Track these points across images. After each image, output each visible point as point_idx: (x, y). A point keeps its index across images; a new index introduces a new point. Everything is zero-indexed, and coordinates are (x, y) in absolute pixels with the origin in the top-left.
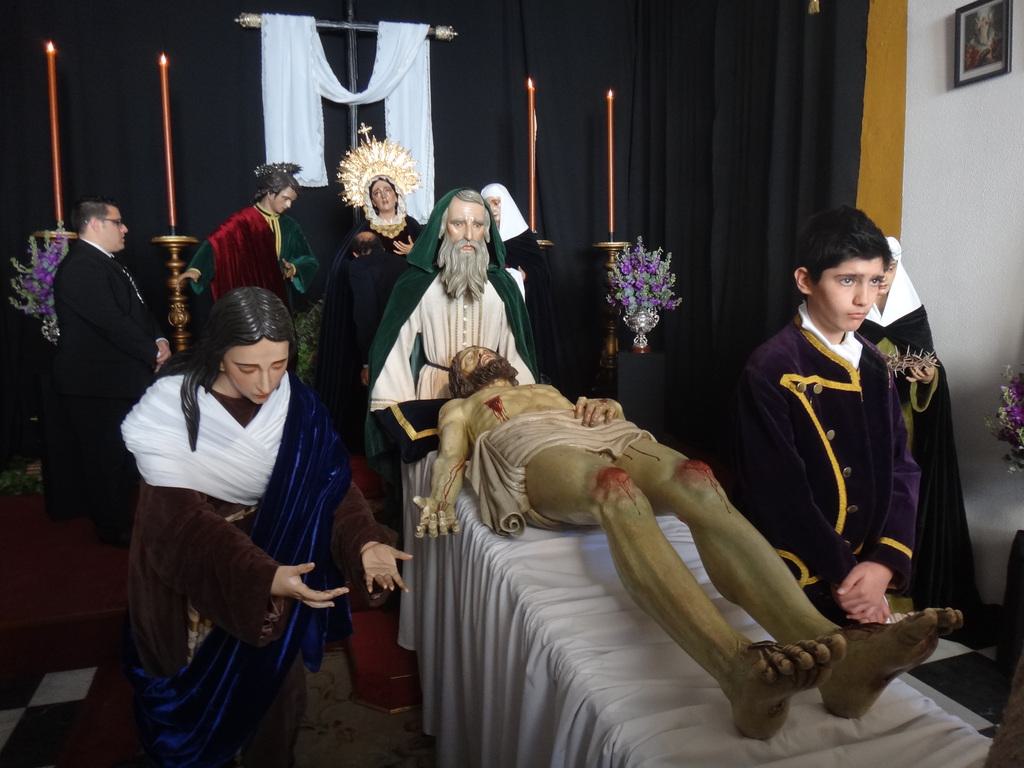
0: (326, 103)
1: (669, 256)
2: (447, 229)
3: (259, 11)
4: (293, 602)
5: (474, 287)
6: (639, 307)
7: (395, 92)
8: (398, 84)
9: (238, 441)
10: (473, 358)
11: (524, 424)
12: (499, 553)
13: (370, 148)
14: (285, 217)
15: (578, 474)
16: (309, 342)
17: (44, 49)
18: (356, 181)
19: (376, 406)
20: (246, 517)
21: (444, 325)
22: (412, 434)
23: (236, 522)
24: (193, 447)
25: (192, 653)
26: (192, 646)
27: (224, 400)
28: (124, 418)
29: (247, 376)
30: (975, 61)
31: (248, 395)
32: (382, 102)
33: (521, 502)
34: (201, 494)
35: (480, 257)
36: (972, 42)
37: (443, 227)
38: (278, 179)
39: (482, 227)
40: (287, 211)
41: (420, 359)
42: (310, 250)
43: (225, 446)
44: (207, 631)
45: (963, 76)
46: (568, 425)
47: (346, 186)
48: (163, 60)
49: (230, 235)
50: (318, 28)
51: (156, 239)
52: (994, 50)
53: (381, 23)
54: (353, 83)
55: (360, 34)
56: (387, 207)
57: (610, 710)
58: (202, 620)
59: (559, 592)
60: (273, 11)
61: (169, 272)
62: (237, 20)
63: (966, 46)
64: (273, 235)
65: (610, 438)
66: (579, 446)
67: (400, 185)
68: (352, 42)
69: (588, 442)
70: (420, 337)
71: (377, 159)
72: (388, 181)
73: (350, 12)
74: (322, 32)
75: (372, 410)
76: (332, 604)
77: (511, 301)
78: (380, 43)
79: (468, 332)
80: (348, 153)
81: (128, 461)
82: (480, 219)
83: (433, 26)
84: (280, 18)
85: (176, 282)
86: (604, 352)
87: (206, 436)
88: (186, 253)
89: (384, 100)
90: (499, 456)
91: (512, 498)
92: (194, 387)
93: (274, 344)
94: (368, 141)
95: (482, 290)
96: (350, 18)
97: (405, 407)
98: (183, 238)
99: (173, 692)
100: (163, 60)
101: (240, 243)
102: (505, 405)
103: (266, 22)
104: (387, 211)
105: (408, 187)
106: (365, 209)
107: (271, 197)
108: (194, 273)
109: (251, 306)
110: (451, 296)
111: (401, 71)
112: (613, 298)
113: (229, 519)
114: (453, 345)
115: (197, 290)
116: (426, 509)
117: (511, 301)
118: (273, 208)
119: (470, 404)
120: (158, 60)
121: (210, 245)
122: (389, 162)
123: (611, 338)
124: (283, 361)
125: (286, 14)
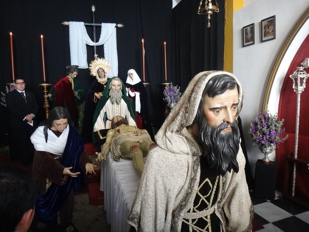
0: (87, 46)
1: (180, 87)
2: (111, 87)
3: (68, 21)
4: (69, 176)
5: (118, 101)
6: (171, 102)
7: (107, 42)
8: (108, 40)
9: (57, 140)
10: (117, 119)
11: (122, 136)
12: (114, 165)
13: (97, 60)
14: (74, 79)
15: (128, 147)
16: (83, 112)
17: (9, 34)
18: (94, 69)
19: (95, 131)
20: (59, 158)
21: (111, 111)
22: (101, 138)
23: (57, 159)
24: (47, 142)
25: (47, 189)
26: (47, 188)
27: (53, 131)
28: (31, 136)
29: (58, 126)
30: (247, 41)
31: (58, 130)
32: (103, 45)
33: (119, 153)
34: (48, 152)
35: (119, 93)
36: (246, 36)
37: (110, 86)
38: (73, 69)
39: (120, 86)
40: (75, 78)
41: (106, 119)
42: (82, 88)
43: (54, 142)
44: (51, 184)
45: (245, 44)
46: (132, 136)
47: (91, 71)
48: (42, 36)
49: (60, 84)
50: (85, 25)
51: (40, 85)
52: (251, 38)
53: (102, 23)
54: (95, 40)
55: (96, 26)
56: (102, 76)
57: (125, 192)
58: (49, 182)
59: (124, 172)
60: (72, 21)
61: (44, 93)
62: (62, 23)
63: (245, 37)
64: (72, 84)
65: (140, 139)
66: (132, 141)
67: (106, 70)
68: (94, 29)
69: (134, 140)
70: (106, 113)
71: (99, 63)
72: (102, 69)
73: (94, 20)
74: (86, 26)
75: (94, 131)
76: (77, 176)
77: (128, 104)
78: (102, 29)
79: (118, 112)
80: (92, 62)
81: (32, 145)
82: (119, 84)
83: (117, 24)
84: (74, 23)
85: (46, 96)
86: (165, 113)
87: (50, 140)
88: (48, 88)
89: (103, 44)
90: (116, 142)
91: (118, 152)
92: (46, 129)
93: (64, 119)
94: (97, 59)
95: (120, 101)
96: (94, 22)
97: (101, 131)
98: (47, 84)
99: (43, 199)
100: (42, 36)
101: (62, 86)
102: (121, 131)
103: (71, 24)
104: (102, 77)
105: (108, 71)
106: (96, 77)
107: (71, 74)
108: (50, 95)
109: (59, 111)
110: (113, 103)
111: (108, 37)
112: (165, 99)
113: (55, 158)
114: (114, 115)
115: (51, 100)
116: (99, 155)
117: (128, 104)
118: (72, 77)
119: (114, 131)
120: (40, 36)
121: (54, 87)
122: (103, 64)
123: (167, 110)
124: (66, 123)
125: (76, 21)
